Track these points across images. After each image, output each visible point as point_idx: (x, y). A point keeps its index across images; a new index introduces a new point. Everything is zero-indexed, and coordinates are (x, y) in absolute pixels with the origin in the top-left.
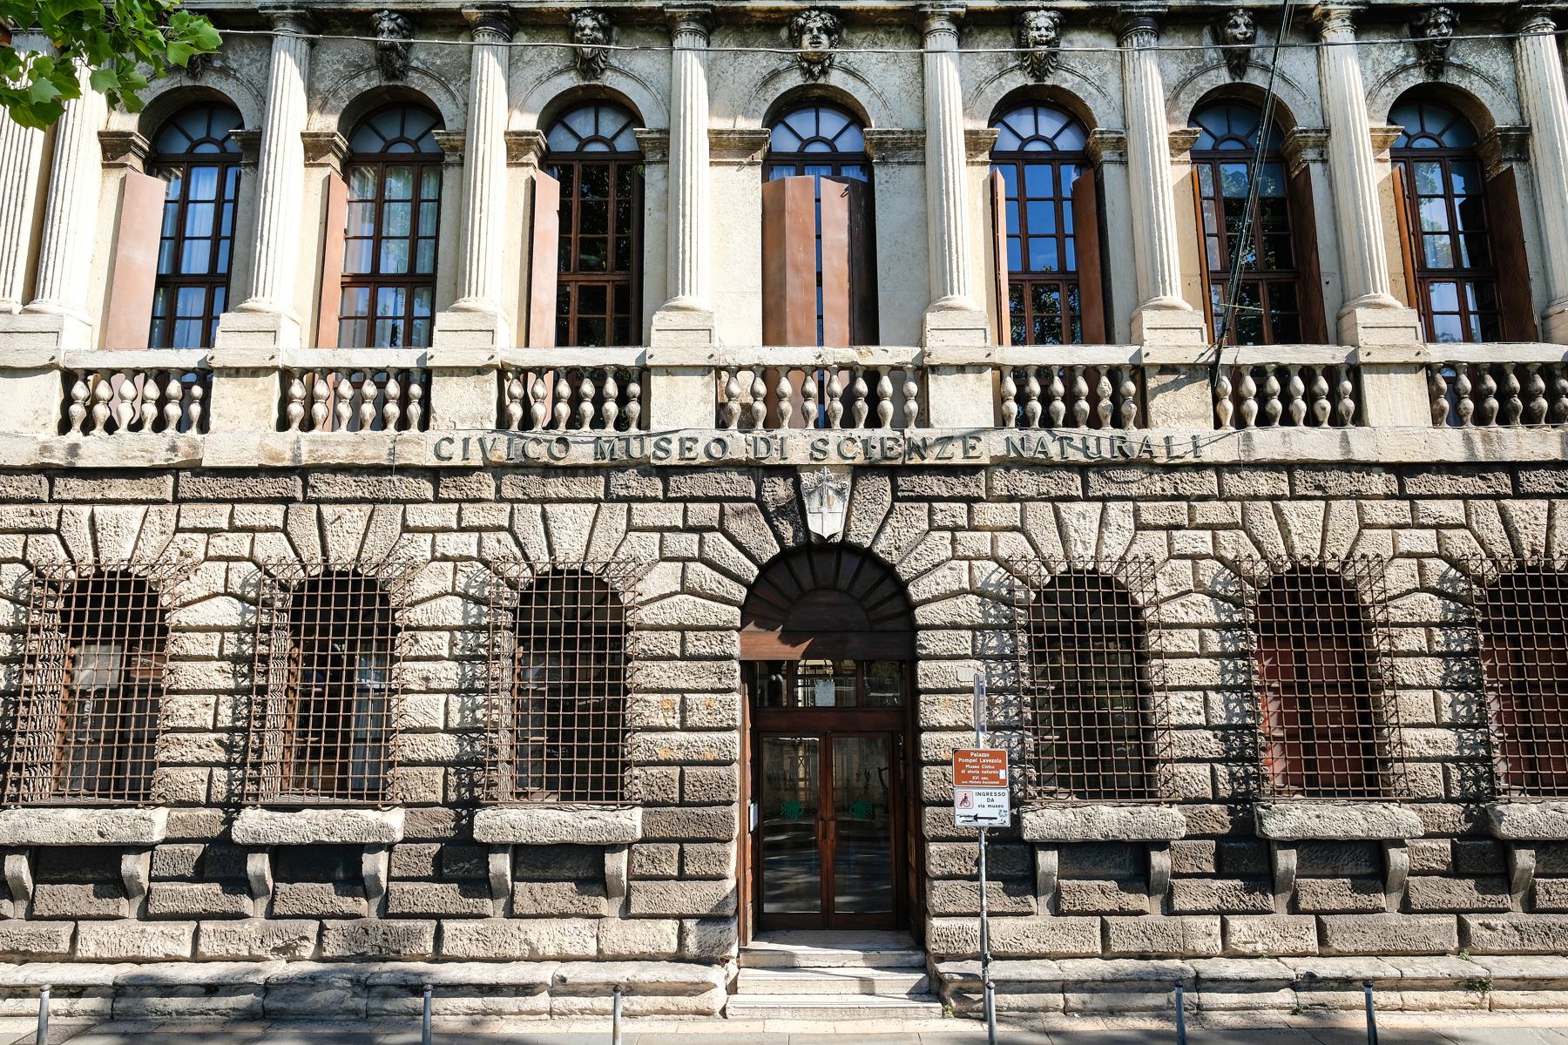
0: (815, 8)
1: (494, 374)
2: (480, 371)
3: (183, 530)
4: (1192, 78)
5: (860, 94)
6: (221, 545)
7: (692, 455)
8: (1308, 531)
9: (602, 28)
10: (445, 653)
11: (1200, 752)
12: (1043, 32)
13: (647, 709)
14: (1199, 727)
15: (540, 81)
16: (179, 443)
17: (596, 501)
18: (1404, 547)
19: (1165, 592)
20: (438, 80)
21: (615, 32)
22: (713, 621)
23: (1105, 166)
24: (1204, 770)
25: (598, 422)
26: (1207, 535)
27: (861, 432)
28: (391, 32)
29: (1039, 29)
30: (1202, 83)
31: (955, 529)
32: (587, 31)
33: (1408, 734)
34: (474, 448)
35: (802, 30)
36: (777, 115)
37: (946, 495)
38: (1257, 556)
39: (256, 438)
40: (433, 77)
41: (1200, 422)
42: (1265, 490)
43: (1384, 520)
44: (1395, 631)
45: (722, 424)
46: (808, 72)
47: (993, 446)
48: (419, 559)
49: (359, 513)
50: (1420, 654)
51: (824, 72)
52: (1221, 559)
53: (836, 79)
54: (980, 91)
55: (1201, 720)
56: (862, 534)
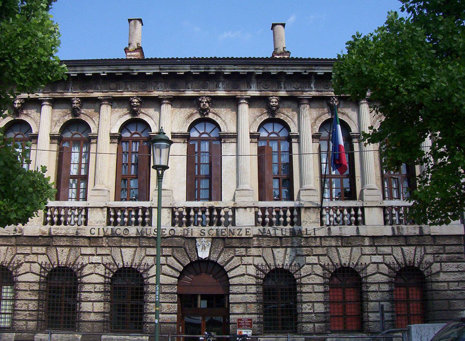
0: (204, 96)
1: (106, 209)
2: (102, 208)
3: (18, 254)
4: (320, 117)
5: (219, 121)
6: (28, 258)
7: (165, 234)
8: (345, 256)
9: (139, 102)
10: (93, 290)
11: (311, 320)
12: (274, 103)
13: (151, 307)
14: (311, 313)
15: (120, 117)
16: (17, 229)
17: (136, 247)
18: (373, 261)
19: (303, 274)
20: (89, 117)
21: (143, 103)
22: (170, 282)
23: (293, 144)
24: (311, 325)
25: (137, 223)
26: (316, 258)
27: (214, 227)
28: (77, 104)
29: (273, 102)
30: (323, 118)
31: (241, 256)
32: (135, 103)
33: (370, 315)
34: (101, 230)
35: (201, 102)
36: (192, 126)
37: (240, 246)
38: (330, 264)
39: (39, 227)
40: (88, 116)
41: (316, 224)
42: (334, 244)
43: (368, 253)
44: (368, 285)
45: (173, 224)
46: (201, 114)
47: (255, 231)
48: (84, 264)
49: (66, 250)
50: (376, 291)
51: (207, 114)
52: (320, 265)
53: (211, 116)
54: (255, 120)
55: (312, 311)
56: (214, 257)
